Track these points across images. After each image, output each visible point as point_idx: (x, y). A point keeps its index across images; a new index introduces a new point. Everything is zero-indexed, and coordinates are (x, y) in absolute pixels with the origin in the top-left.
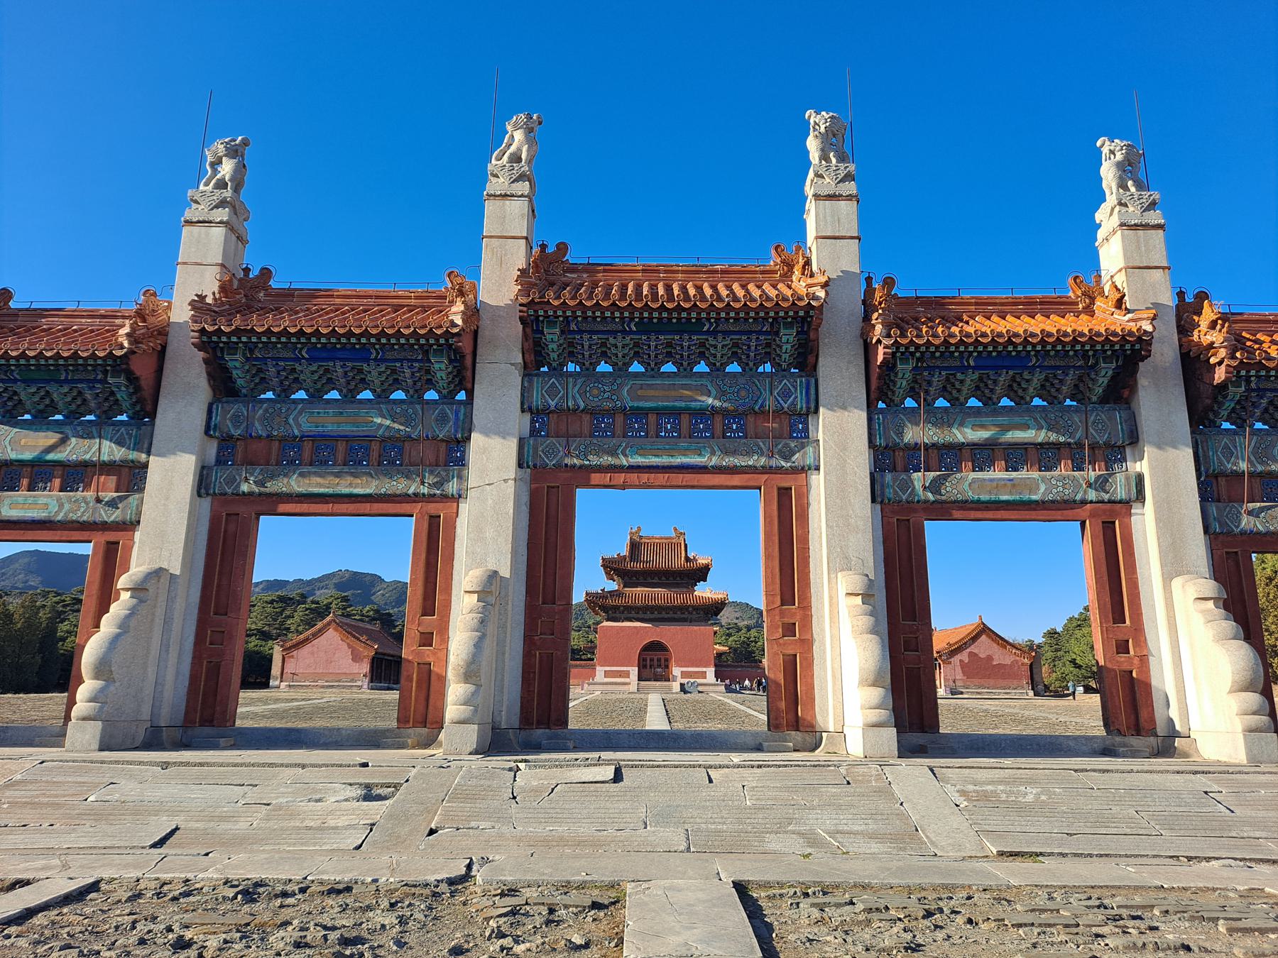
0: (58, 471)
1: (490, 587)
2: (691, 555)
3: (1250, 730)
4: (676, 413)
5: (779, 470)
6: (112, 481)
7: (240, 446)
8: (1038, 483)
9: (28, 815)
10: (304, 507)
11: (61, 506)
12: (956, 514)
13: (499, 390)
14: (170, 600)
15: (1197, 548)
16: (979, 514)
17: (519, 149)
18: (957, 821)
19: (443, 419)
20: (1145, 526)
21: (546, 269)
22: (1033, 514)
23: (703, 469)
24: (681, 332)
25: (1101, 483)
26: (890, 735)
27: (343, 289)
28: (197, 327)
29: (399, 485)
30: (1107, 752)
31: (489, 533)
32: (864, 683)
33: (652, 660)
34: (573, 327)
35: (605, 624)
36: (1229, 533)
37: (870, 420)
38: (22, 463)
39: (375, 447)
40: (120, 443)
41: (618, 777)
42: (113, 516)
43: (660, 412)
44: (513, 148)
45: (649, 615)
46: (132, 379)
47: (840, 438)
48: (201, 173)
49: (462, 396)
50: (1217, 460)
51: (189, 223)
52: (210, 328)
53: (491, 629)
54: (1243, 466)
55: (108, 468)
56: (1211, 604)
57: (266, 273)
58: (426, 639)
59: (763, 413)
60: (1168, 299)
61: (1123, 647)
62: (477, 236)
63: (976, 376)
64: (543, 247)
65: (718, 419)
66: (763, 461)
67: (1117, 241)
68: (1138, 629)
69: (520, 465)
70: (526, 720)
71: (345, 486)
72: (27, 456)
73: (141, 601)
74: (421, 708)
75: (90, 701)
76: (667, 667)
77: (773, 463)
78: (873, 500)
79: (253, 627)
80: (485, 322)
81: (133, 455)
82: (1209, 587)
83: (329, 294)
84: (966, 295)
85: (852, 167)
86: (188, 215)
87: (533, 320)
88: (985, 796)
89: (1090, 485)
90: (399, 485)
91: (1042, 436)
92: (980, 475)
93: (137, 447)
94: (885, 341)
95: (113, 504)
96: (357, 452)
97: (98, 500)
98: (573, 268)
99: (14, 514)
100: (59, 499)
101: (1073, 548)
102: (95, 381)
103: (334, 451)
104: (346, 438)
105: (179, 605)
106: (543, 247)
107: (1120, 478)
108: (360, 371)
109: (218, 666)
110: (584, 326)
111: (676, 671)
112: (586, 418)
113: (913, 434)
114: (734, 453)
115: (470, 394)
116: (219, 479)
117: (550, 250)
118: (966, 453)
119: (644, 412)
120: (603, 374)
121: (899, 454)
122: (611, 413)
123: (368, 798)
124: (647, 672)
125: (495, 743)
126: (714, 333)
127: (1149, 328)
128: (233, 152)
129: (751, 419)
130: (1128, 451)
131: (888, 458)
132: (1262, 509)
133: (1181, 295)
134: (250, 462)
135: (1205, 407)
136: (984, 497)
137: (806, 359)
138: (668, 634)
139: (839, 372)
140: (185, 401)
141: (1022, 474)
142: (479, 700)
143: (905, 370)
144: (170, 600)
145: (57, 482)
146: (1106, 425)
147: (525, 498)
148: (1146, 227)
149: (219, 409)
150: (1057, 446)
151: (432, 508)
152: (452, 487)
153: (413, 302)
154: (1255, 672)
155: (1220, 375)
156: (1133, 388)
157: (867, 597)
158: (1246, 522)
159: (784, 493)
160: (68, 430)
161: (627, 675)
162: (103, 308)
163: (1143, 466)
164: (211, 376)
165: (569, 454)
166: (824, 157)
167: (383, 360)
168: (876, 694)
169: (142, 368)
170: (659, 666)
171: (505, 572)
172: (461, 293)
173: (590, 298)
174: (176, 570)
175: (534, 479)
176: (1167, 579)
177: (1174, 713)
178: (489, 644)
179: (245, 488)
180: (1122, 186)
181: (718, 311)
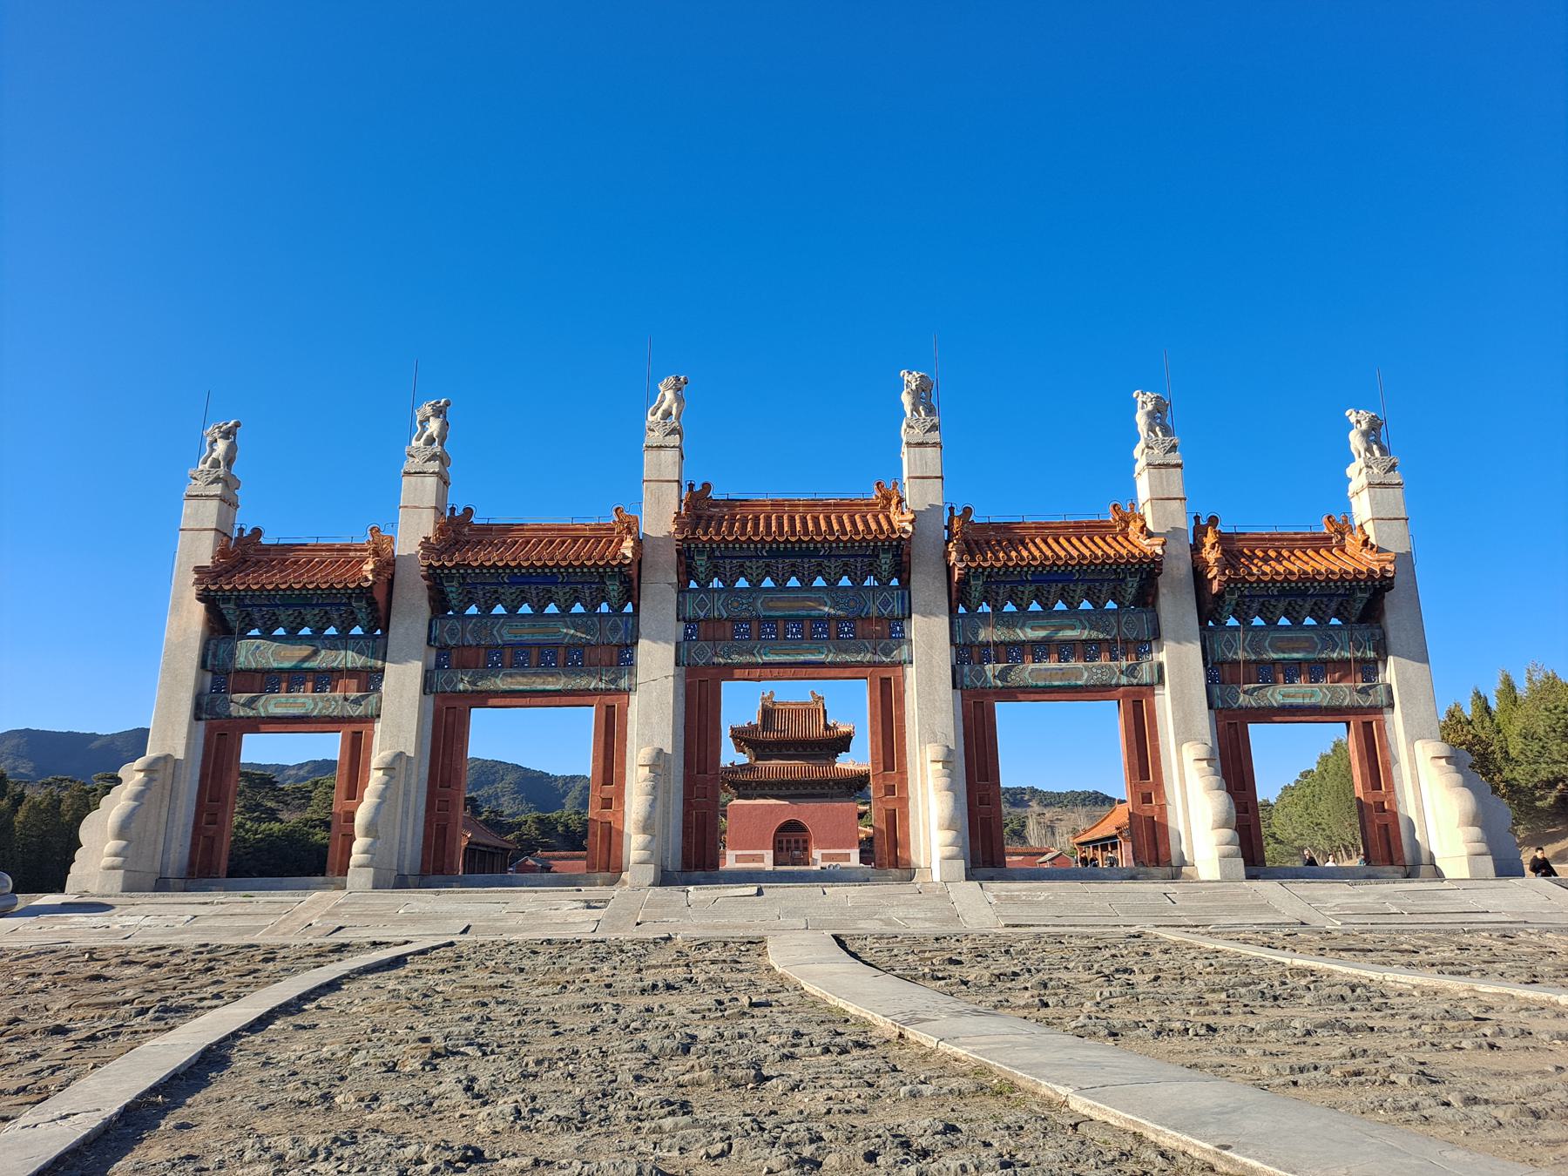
0: (310, 676)
1: (658, 762)
2: (831, 722)
3: (1224, 856)
4: (798, 620)
5: (881, 664)
6: (354, 683)
7: (454, 653)
8: (1082, 671)
9: (368, 921)
10: (507, 701)
11: (316, 704)
12: (1021, 696)
13: (660, 602)
14: (408, 776)
15: (1202, 720)
16: (1037, 697)
17: (670, 407)
18: (989, 911)
19: (615, 629)
20: (1164, 703)
21: (698, 508)
22: (1079, 696)
23: (821, 665)
24: (802, 557)
25: (1131, 671)
26: (960, 865)
27: (530, 521)
28: (426, 563)
29: (582, 683)
30: (1133, 878)
31: (655, 719)
32: (941, 827)
33: (788, 842)
34: (717, 553)
35: (736, 802)
36: (1230, 708)
37: (951, 624)
38: (281, 670)
39: (561, 651)
40: (360, 652)
41: (760, 893)
42: (359, 711)
43: (787, 619)
44: (665, 406)
45: (784, 792)
46: (372, 603)
47: (928, 637)
48: (412, 430)
49: (629, 608)
50: (1221, 651)
51: (408, 474)
52: (436, 564)
53: (660, 793)
54: (1241, 656)
55: (352, 673)
56: (1443, 762)
57: (468, 512)
58: (607, 804)
59: (868, 618)
60: (1184, 523)
61: (1147, 799)
62: (637, 480)
63: (1033, 588)
64: (691, 486)
65: (833, 624)
66: (868, 657)
67: (1145, 475)
68: (1159, 784)
69: (677, 664)
70: (687, 865)
71: (539, 684)
72: (286, 665)
73: (392, 778)
74: (605, 856)
75: (364, 852)
76: (806, 849)
77: (877, 658)
78: (954, 687)
79: (315, 817)
80: (647, 550)
81: (371, 662)
82: (1441, 748)
83: (520, 527)
84: (1028, 520)
85: (936, 420)
86: (407, 467)
87: (686, 556)
88: (1012, 897)
89: (1122, 672)
90: (582, 683)
91: (1085, 635)
92: (1037, 666)
93: (374, 656)
94: (960, 565)
95: (357, 702)
96: (549, 656)
97: (346, 699)
98: (716, 503)
99: (279, 711)
100: (314, 699)
101: (1110, 718)
102: (341, 604)
103: (528, 655)
104: (539, 645)
105: (414, 781)
106: (691, 486)
107: (1145, 666)
108: (549, 591)
109: (445, 828)
110: (726, 554)
111: (816, 854)
112: (728, 624)
113: (985, 635)
114: (846, 652)
115: (636, 607)
116: (440, 679)
117: (697, 488)
118: (1028, 648)
119: (775, 619)
120: (741, 589)
121: (975, 650)
122: (748, 621)
123: (589, 907)
124: (783, 856)
125: (665, 879)
126: (828, 557)
127: (1160, 552)
128: (439, 412)
129: (859, 623)
130: (1154, 644)
131: (966, 653)
132: (1255, 689)
133: (1197, 518)
134: (463, 666)
135: (1209, 609)
136: (1041, 683)
137: (902, 570)
138: (807, 812)
139: (927, 586)
140: (411, 618)
141: (1072, 664)
142: (654, 846)
143: (977, 585)
144: (408, 776)
145: (310, 685)
146: (1134, 625)
147: (682, 691)
148: (1167, 466)
149: (437, 624)
150: (1098, 642)
151: (608, 700)
152: (624, 683)
153: (588, 533)
154: (1229, 813)
155: (1215, 587)
156: (1156, 596)
157: (946, 763)
158: (1243, 700)
159: (886, 682)
160: (318, 643)
161: (761, 859)
162: (338, 542)
163: (1162, 657)
164: (431, 599)
165: (716, 654)
166: (915, 409)
167: (568, 583)
168: (949, 835)
169: (379, 596)
170: (797, 849)
171: (668, 750)
172: (630, 532)
173: (730, 534)
174: (180, 754)
175: (688, 675)
176: (1179, 745)
177: (1184, 848)
178: (659, 804)
179: (461, 687)
180: (1151, 429)
181: (830, 542)
